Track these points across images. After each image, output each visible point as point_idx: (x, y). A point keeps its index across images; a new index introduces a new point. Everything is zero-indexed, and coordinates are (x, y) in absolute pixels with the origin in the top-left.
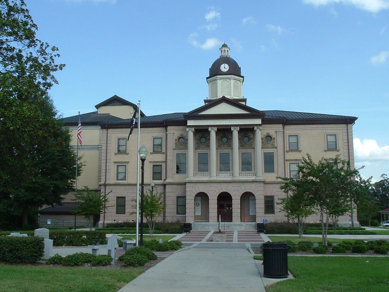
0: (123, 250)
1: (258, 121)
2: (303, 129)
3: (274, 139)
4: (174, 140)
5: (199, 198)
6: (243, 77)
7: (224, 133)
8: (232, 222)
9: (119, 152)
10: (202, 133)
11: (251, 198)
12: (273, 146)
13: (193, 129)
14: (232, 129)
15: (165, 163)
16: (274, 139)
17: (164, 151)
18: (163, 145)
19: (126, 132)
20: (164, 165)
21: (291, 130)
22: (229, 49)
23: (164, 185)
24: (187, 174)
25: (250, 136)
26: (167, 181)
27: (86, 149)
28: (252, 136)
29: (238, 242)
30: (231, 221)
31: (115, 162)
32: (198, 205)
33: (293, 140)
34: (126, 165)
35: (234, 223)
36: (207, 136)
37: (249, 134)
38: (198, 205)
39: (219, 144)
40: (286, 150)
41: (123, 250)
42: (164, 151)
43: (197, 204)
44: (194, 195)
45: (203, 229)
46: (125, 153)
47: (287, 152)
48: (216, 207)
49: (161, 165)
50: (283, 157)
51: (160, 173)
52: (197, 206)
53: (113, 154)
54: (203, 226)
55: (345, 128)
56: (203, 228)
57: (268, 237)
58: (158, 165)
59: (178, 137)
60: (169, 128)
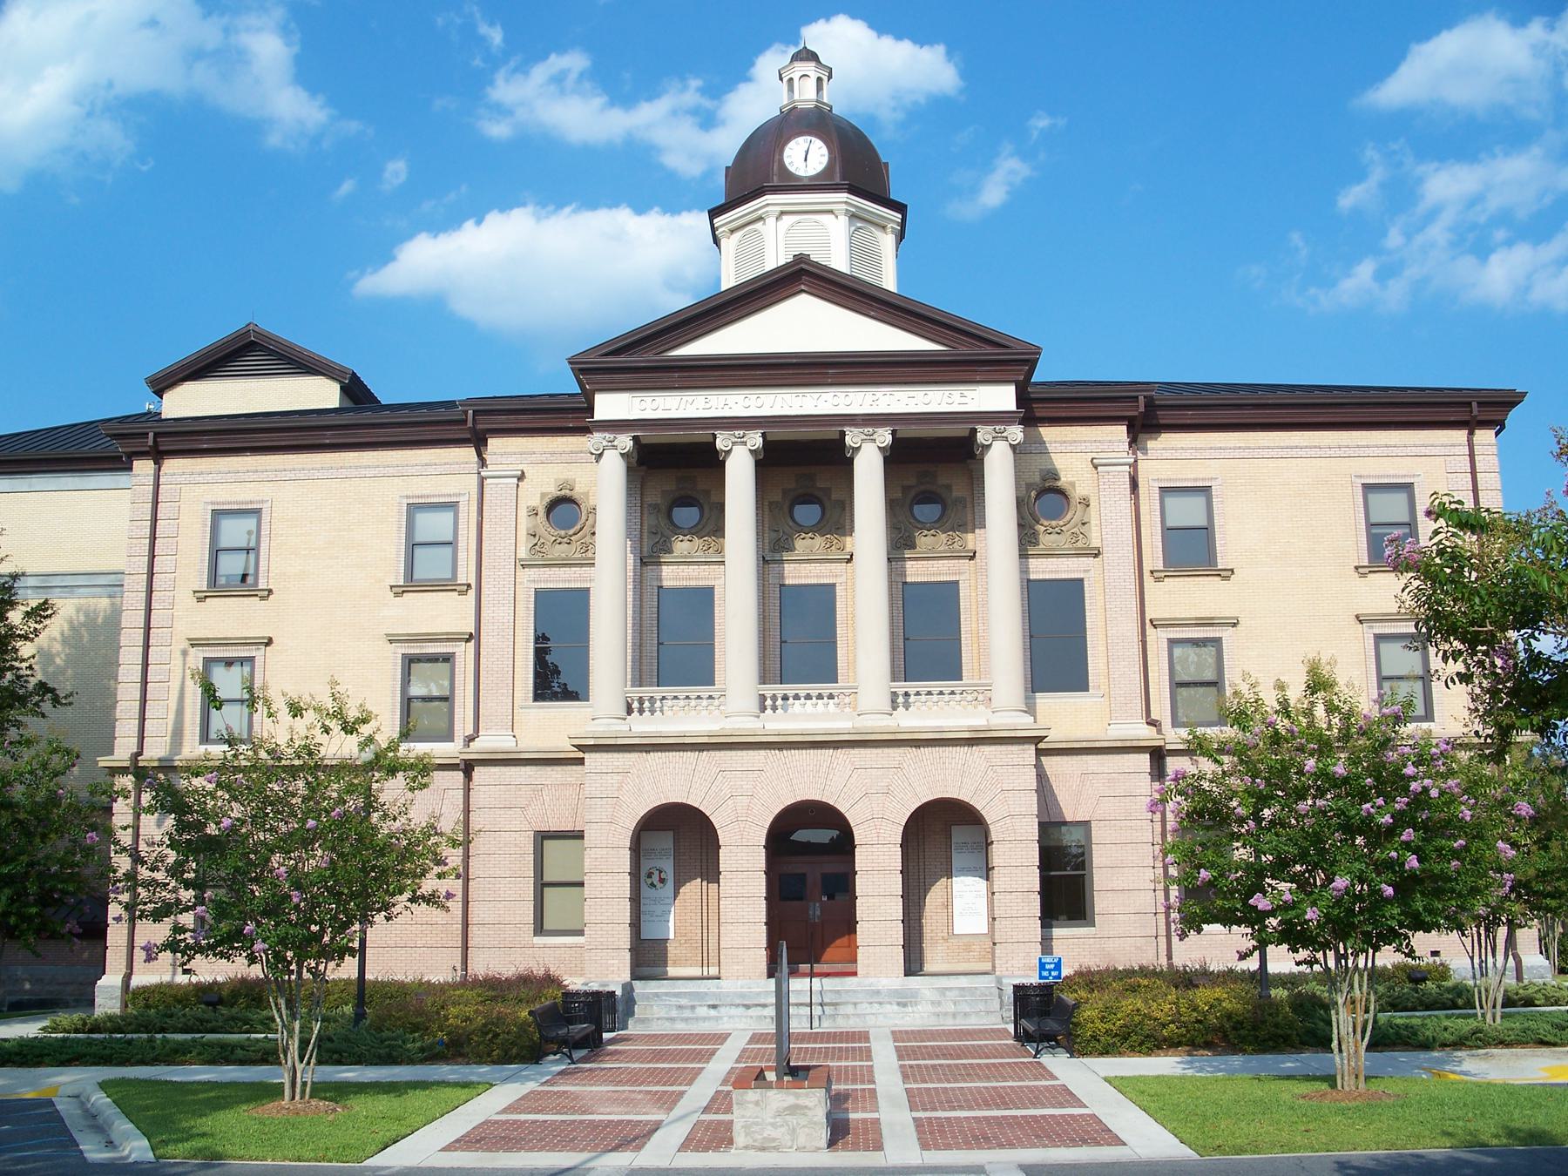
0: (987, 872)
1: (1002, 397)
2: (1237, 454)
3: (1085, 503)
4: (523, 513)
5: (665, 841)
6: (900, 208)
7: (804, 472)
8: (855, 974)
9: (215, 587)
10: (675, 475)
11: (959, 834)
12: (1079, 544)
13: (625, 442)
14: (852, 437)
15: (472, 644)
16: (1085, 503)
17: (466, 574)
18: (462, 544)
19: (255, 477)
20: (464, 653)
21: (1177, 455)
22: (830, 77)
23: (468, 768)
24: (405, 501)
25: (949, 487)
26: (488, 742)
27: (82, 590)
28: (958, 491)
29: (925, 1146)
30: (848, 967)
31: (195, 643)
32: (655, 878)
33: (1187, 512)
34: (251, 659)
35: (868, 981)
36: (707, 493)
37: (943, 480)
38: (655, 878)
39: (774, 535)
40: (1147, 568)
41: (987, 872)
42: (466, 574)
43: (650, 875)
44: (631, 824)
45: (686, 1020)
46: (245, 585)
47: (1158, 580)
48: (761, 890)
49: (448, 658)
50: (1133, 604)
51: (444, 699)
52: (653, 885)
53: (185, 598)
54: (683, 1002)
55: (1457, 450)
56: (687, 1013)
57: (1115, 1082)
58: (433, 659)
59: (543, 495)
60: (494, 444)
